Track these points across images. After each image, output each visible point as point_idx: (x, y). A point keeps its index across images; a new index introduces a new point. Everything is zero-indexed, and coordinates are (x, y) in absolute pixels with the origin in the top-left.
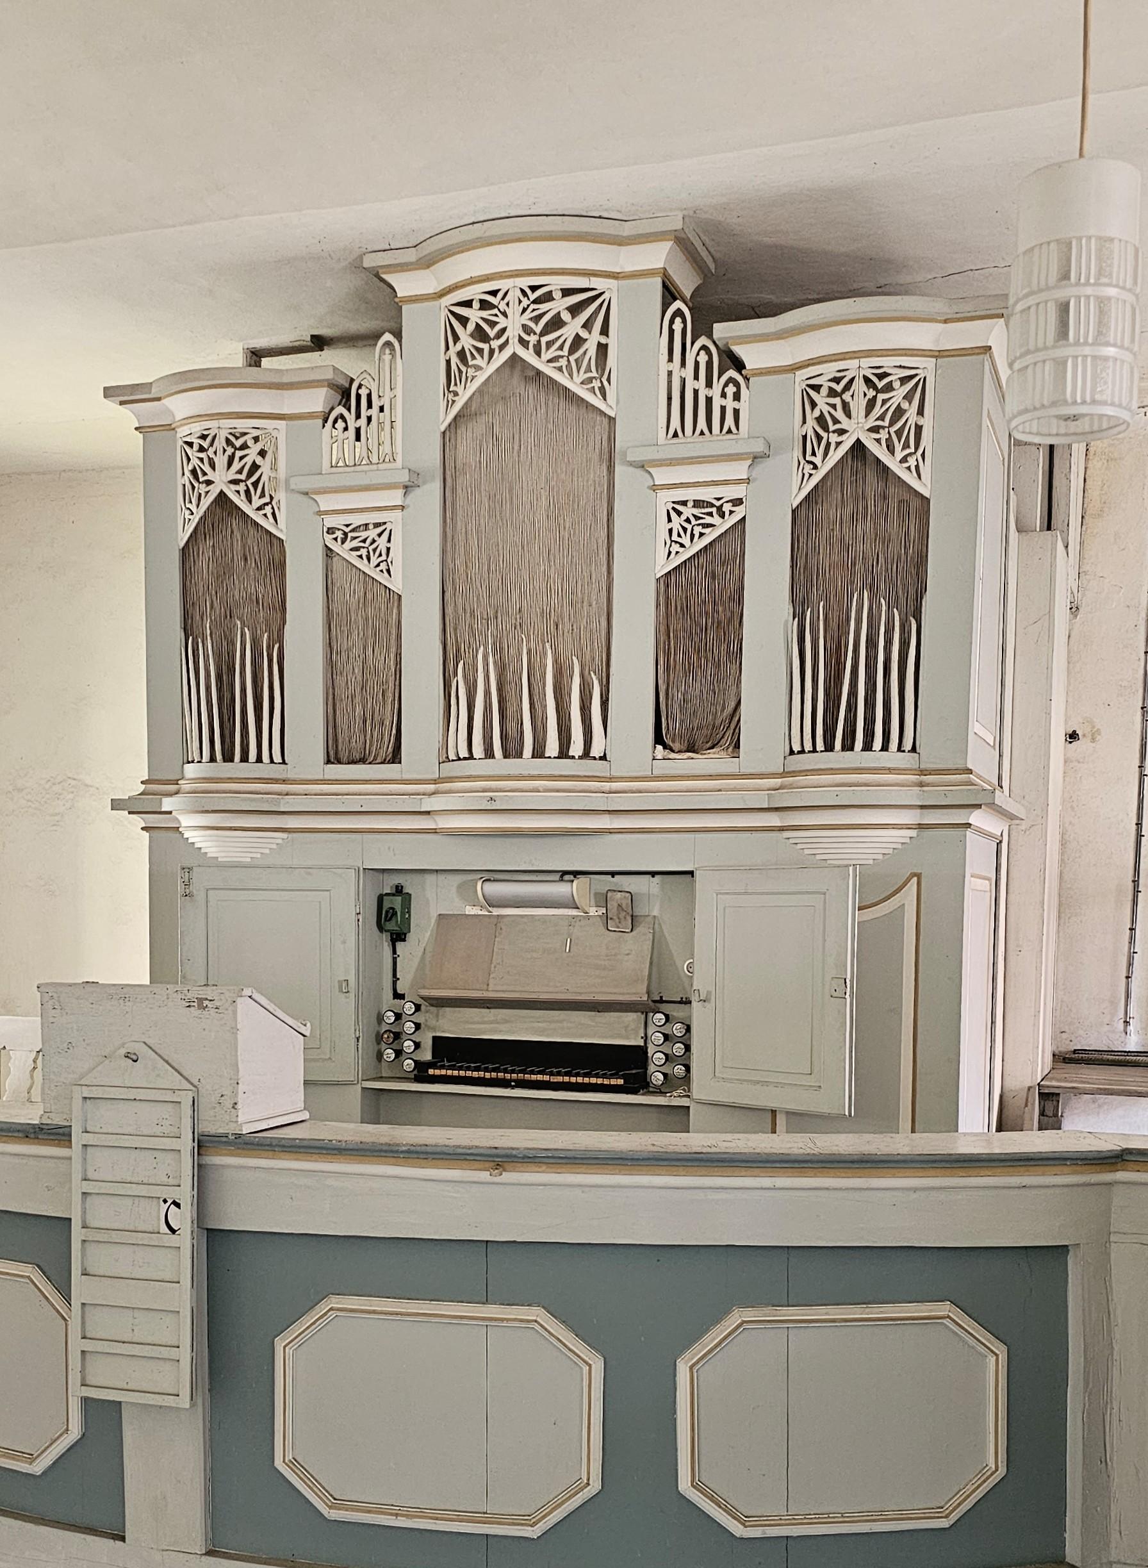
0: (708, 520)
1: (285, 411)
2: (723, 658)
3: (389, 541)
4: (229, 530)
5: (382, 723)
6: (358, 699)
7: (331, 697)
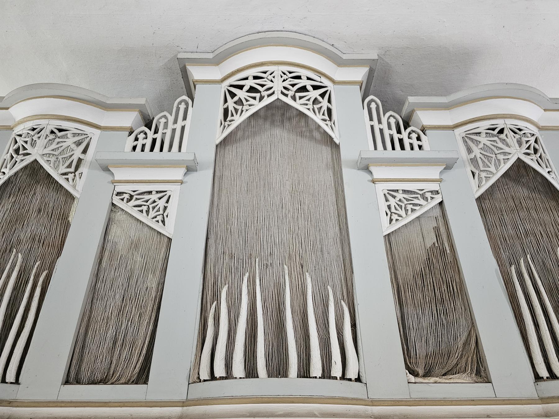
0: (416, 201)
1: (102, 124)
2: (446, 296)
3: (167, 202)
4: (32, 192)
5: (133, 343)
6: (112, 322)
7: (86, 319)
